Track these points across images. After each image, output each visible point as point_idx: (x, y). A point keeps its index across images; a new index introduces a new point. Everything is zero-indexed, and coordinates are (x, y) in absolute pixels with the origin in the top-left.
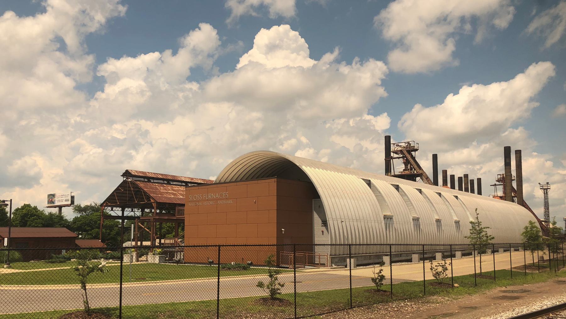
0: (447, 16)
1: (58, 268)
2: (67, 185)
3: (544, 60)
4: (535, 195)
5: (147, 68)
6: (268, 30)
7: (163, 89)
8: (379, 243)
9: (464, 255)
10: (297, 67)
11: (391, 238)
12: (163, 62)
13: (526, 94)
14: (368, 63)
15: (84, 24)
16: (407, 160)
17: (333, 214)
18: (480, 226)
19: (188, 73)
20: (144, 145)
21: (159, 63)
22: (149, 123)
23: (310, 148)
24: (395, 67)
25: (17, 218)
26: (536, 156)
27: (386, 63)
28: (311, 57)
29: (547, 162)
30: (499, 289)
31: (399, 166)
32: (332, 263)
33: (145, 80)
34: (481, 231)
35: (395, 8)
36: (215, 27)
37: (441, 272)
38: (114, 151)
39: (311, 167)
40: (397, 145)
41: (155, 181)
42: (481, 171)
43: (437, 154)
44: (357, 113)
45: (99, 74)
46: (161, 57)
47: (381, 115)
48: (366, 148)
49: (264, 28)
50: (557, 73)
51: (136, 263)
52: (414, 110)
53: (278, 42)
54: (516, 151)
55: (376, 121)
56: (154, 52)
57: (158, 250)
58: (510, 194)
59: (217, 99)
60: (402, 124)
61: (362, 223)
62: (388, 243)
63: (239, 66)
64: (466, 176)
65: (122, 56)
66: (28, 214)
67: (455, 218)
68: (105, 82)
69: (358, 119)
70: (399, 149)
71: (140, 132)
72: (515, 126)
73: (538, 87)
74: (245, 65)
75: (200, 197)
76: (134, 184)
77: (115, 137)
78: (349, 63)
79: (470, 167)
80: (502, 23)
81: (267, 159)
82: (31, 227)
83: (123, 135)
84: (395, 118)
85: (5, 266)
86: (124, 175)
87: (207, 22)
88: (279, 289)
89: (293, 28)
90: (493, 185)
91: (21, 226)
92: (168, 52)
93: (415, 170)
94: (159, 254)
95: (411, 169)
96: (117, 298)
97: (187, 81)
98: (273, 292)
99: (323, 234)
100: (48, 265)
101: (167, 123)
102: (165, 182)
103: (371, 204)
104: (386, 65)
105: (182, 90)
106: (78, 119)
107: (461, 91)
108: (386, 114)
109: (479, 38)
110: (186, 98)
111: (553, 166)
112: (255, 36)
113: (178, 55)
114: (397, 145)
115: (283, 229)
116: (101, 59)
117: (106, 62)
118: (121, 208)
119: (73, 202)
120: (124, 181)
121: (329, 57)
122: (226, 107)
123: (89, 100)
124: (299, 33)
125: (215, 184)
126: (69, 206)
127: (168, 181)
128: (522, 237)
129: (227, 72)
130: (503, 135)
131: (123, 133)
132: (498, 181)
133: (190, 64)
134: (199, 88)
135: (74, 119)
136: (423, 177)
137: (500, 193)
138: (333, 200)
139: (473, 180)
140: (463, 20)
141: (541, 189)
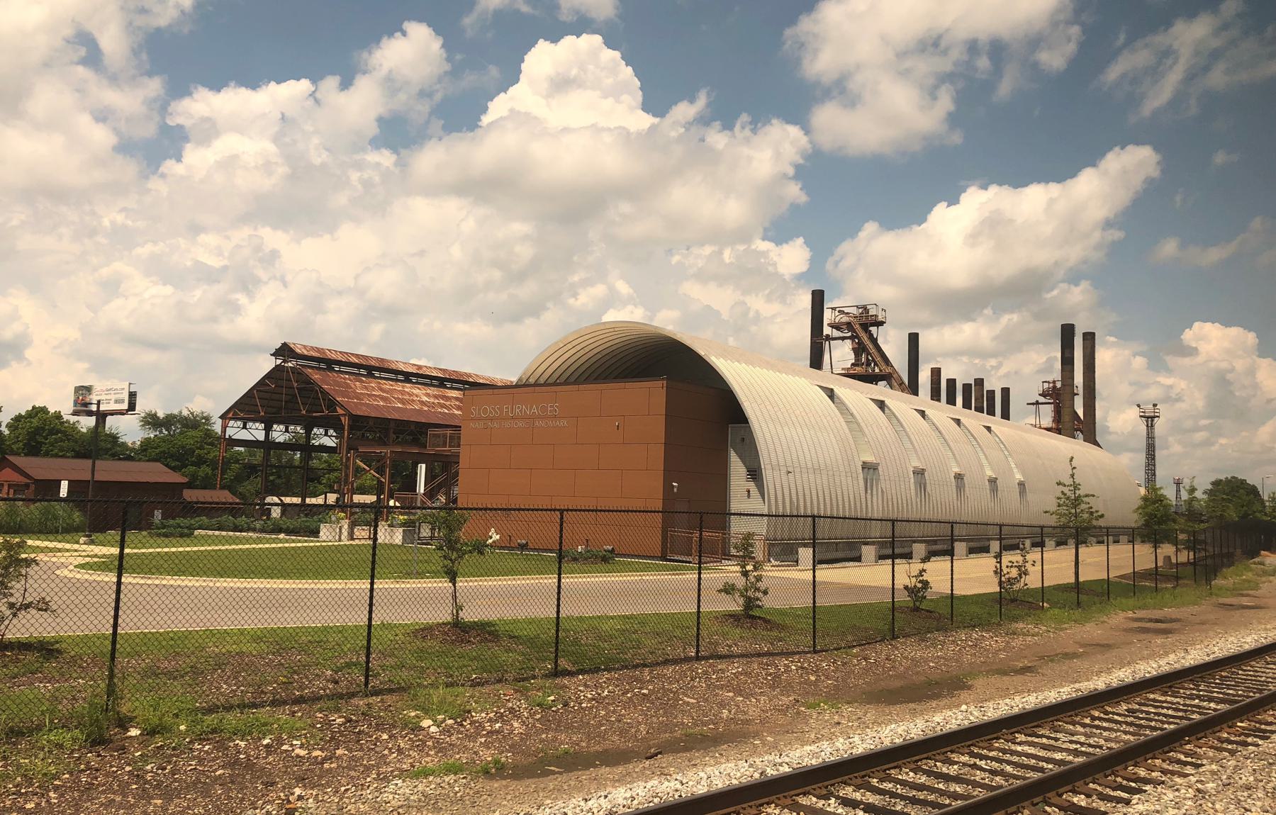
0: (940, 37)
1: (195, 549)
2: (86, 365)
3: (1138, 142)
4: (1109, 427)
5: (283, 114)
6: (553, 45)
7: (317, 161)
8: (853, 515)
9: (972, 551)
10: (615, 128)
11: (875, 508)
12: (317, 101)
13: (1098, 212)
14: (768, 128)
15: (143, 7)
16: (860, 343)
17: (773, 455)
18: (1077, 492)
19: (373, 130)
20: (266, 283)
21: (311, 102)
22: (280, 234)
23: (635, 306)
24: (826, 141)
25: (18, 438)
26: (1113, 345)
27: (807, 130)
28: (647, 107)
30: (1122, 615)
31: (841, 354)
32: (769, 555)
33: (276, 139)
34: (1077, 501)
35: (830, 16)
36: (438, 31)
37: (1016, 578)
38: (198, 294)
39: (725, 357)
40: (839, 311)
41: (384, 374)
42: (1000, 371)
43: (918, 334)
44: (741, 236)
45: (170, 122)
46: (314, 92)
47: (791, 243)
48: (757, 312)
49: (546, 40)
50: (1163, 171)
51: (348, 543)
52: (862, 235)
53: (574, 72)
54: (1085, 334)
55: (779, 255)
56: (298, 80)
57: (401, 517)
59: (435, 190)
60: (836, 264)
61: (825, 477)
62: (809, 513)
63: (486, 120)
64: (979, 382)
65: (226, 85)
66: (43, 429)
67: (989, 473)
68: (186, 139)
69: (741, 248)
70: (845, 319)
71: (260, 254)
72: (1074, 277)
73: (1123, 197)
74: (501, 118)
75: (495, 411)
76: (299, 373)
77: (202, 263)
78: (728, 126)
79: (977, 361)
80: (1054, 59)
81: (628, 338)
82: (51, 457)
83: (221, 258)
84: (821, 252)
85: (82, 540)
86: (277, 354)
87: (420, 20)
88: (758, 599)
89: (610, 43)
90: (1033, 404)
91: (26, 455)
92: (331, 83)
93: (876, 364)
94: (403, 525)
95: (868, 364)
96: (363, 608)
97: (369, 147)
98: (750, 604)
99: (749, 496)
100: (159, 541)
101: (321, 236)
102: (363, 372)
103: (838, 438)
104: (805, 134)
105: (359, 166)
106: (120, 218)
107: (964, 198)
108: (800, 241)
109: (1005, 88)
110: (367, 184)
111: (1148, 368)
112: (525, 57)
113: (352, 89)
114: (839, 311)
115: (674, 484)
116: (179, 90)
117: (190, 94)
118: (263, 425)
119: (132, 407)
120: (276, 366)
121: (684, 111)
122: (453, 208)
123: (147, 178)
124: (622, 54)
125: (517, 386)
126: (124, 414)
127: (371, 369)
128: (1136, 516)
129: (459, 131)
130: (1049, 296)
131: (220, 254)
132: (1043, 395)
133: (380, 110)
134: (396, 164)
135: (111, 217)
137: (1047, 421)
138: (771, 426)
139: (993, 392)
140: (973, 47)
141: (1141, 416)
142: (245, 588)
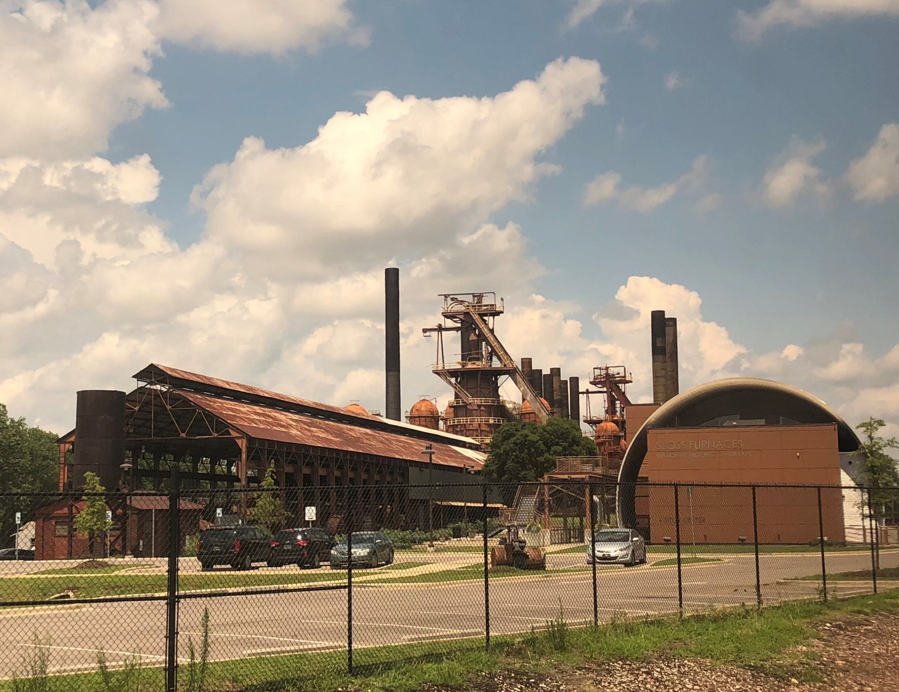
3: (586, 55)
29: (566, 322)
40: (452, 299)
47: (131, 162)
52: (241, 155)
58: (250, 399)
70: (461, 308)
72: (500, 220)
86: (139, 376)
108: (145, 159)
111: (581, 336)
120: (139, 389)
130: (466, 240)
136: (518, 376)
142: (34, 616)
